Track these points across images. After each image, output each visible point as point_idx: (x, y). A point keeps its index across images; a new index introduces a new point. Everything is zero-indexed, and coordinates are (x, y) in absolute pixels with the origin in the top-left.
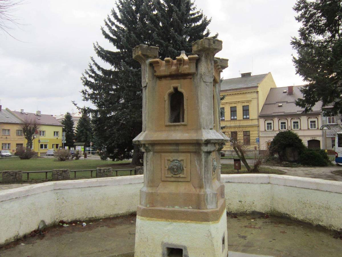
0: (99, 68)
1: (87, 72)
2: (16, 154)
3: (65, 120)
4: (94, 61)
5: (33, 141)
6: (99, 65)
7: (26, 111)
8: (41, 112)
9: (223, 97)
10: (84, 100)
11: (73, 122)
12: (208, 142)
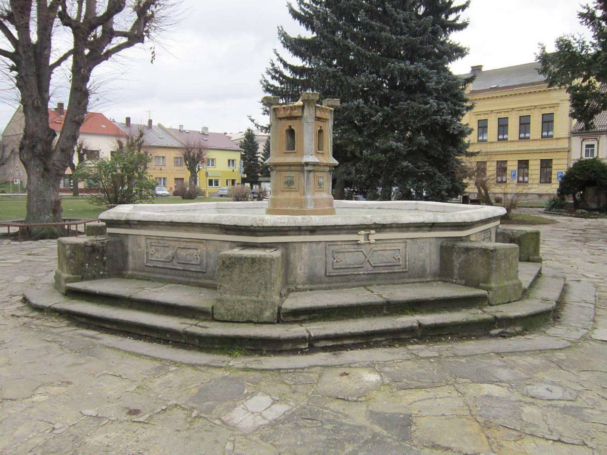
0: (286, 65)
1: (269, 72)
2: (175, 194)
3: (245, 141)
4: (278, 55)
5: (198, 174)
6: (285, 61)
7: (186, 128)
8: (209, 129)
9: (471, 106)
10: (264, 114)
11: (257, 145)
12: (307, 164)
